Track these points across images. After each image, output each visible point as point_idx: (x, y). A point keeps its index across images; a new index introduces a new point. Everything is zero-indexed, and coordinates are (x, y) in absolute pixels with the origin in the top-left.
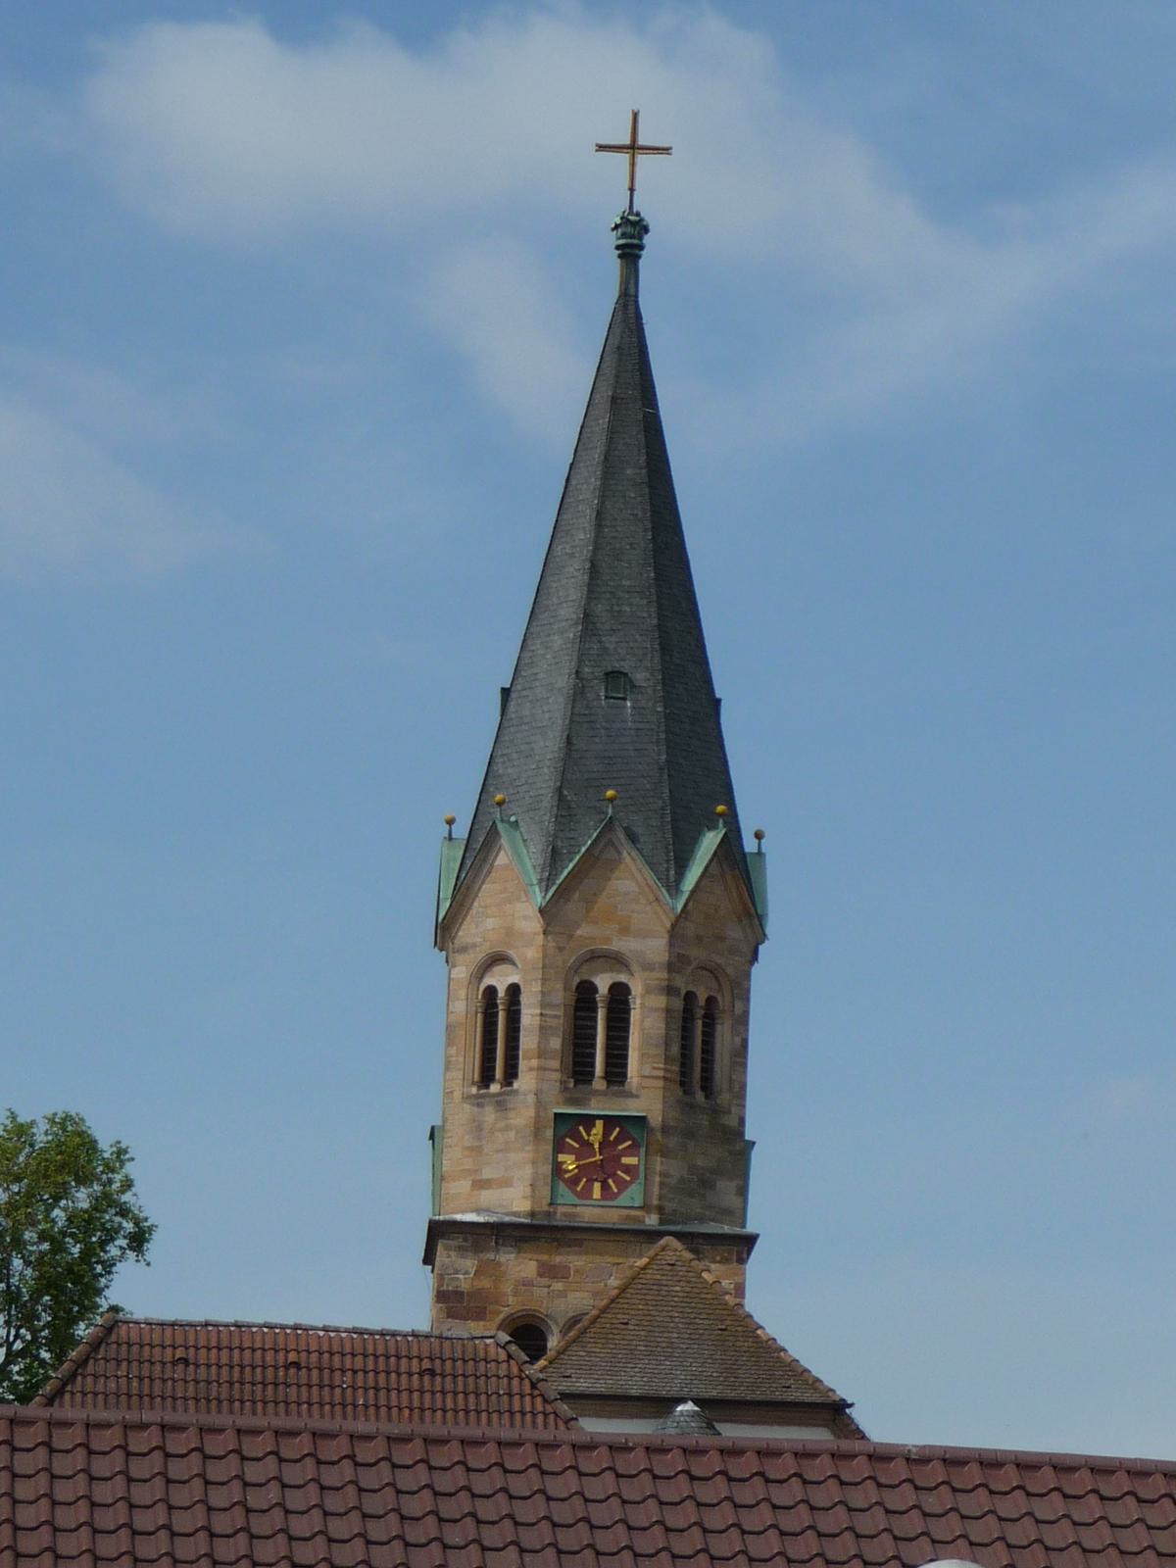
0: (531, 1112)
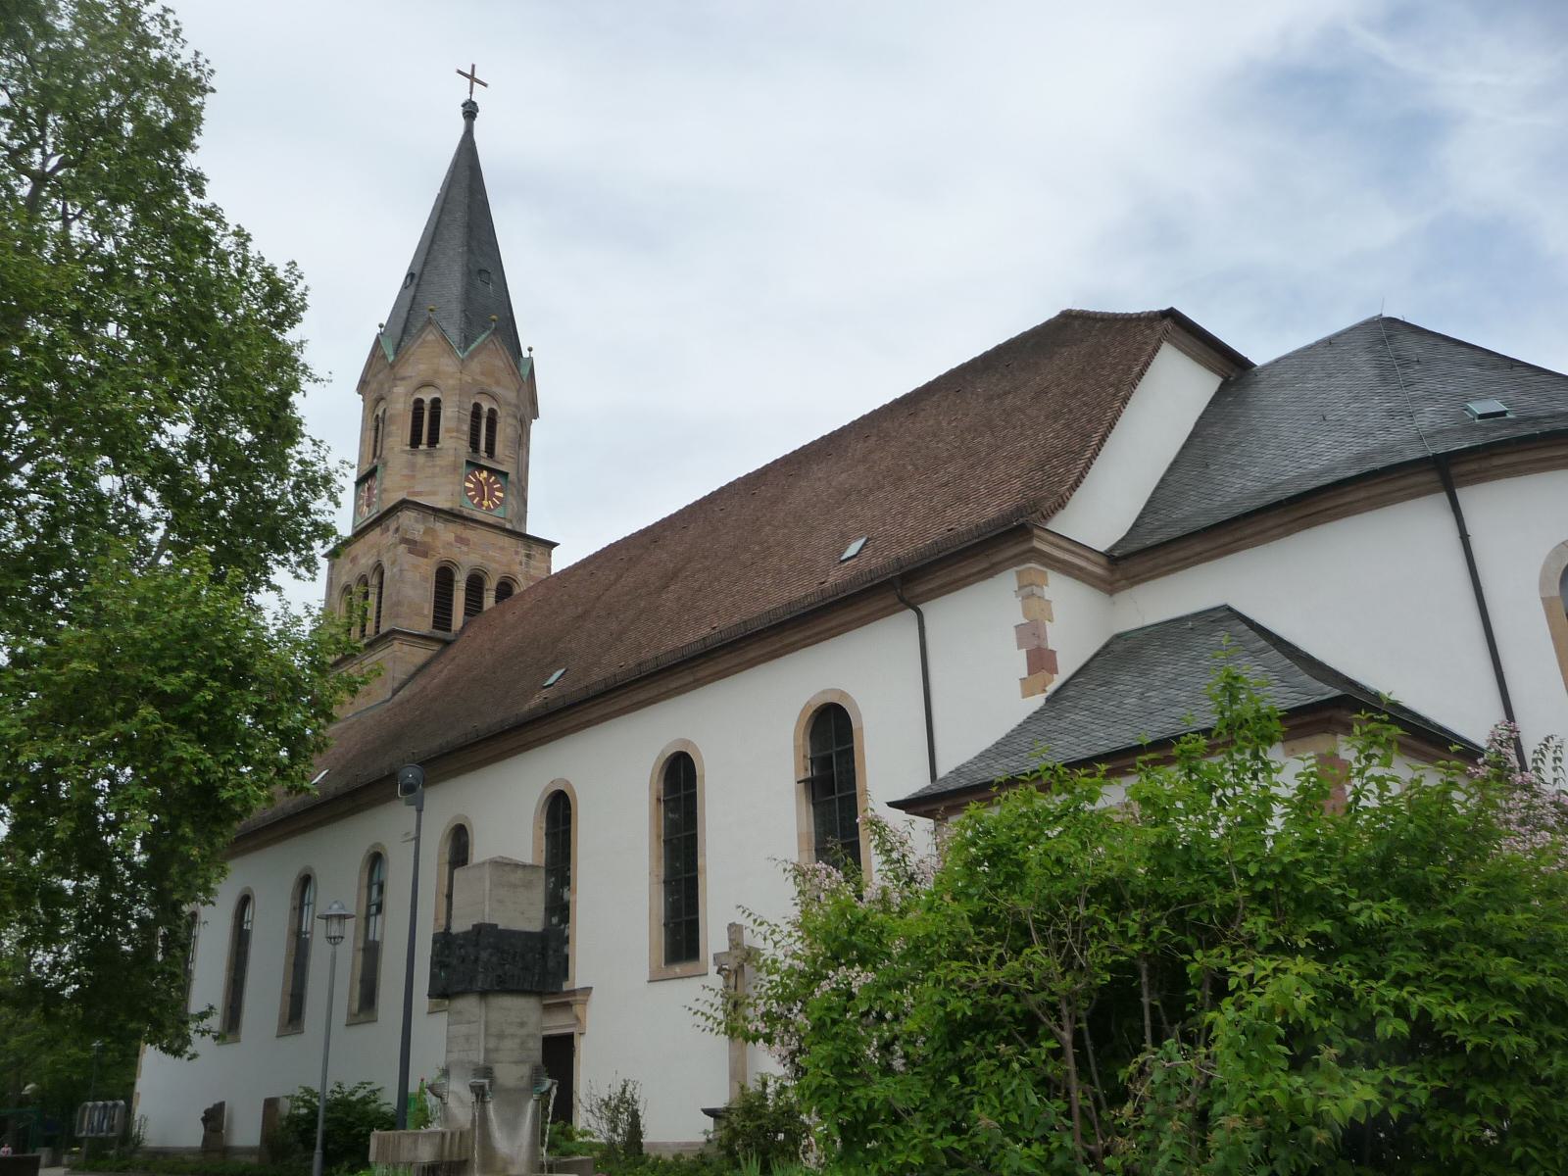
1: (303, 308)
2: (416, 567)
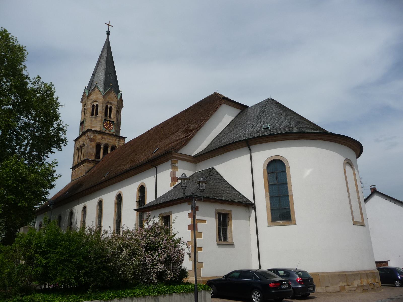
0: (101, 119)
1: (54, 92)
2: (91, 144)
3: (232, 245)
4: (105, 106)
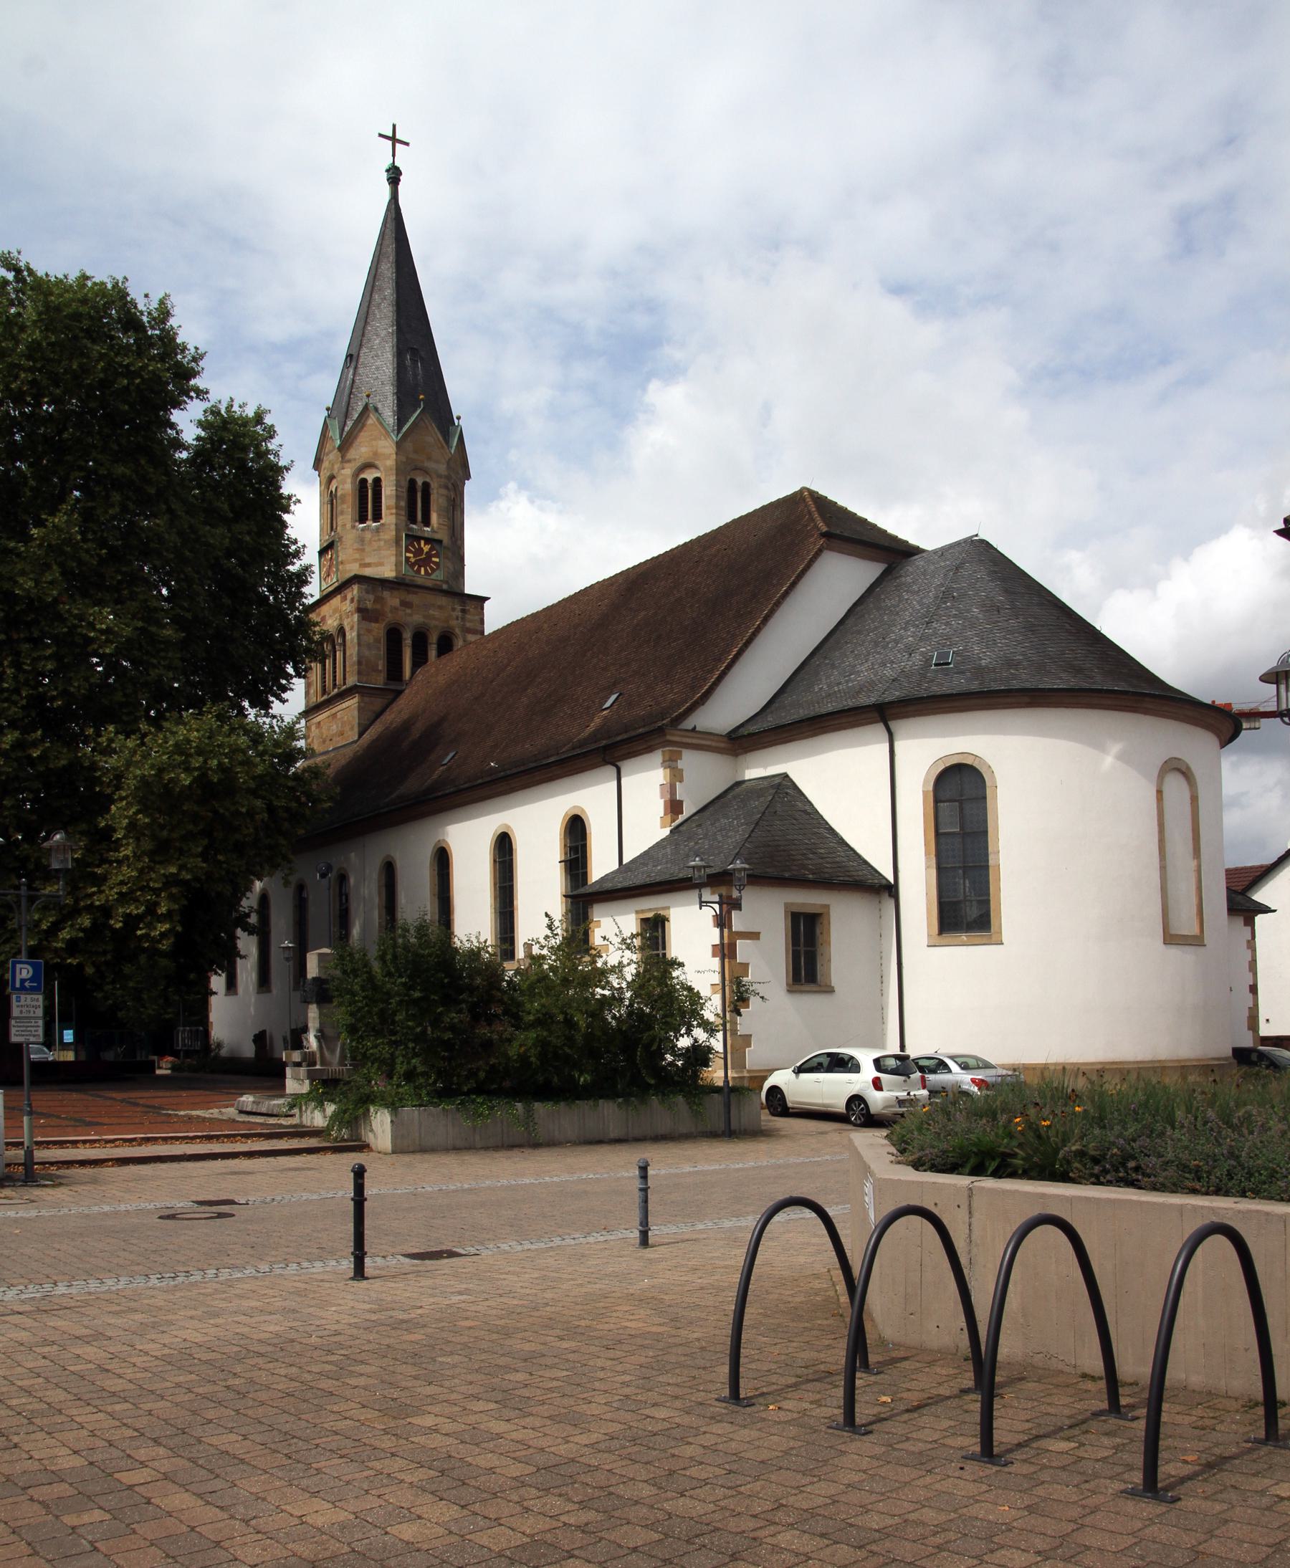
2: (369, 631)
3: (830, 990)
4: (405, 484)
